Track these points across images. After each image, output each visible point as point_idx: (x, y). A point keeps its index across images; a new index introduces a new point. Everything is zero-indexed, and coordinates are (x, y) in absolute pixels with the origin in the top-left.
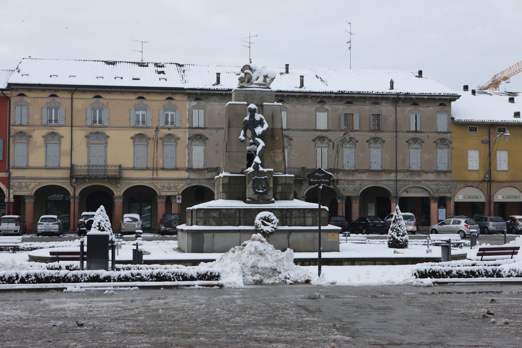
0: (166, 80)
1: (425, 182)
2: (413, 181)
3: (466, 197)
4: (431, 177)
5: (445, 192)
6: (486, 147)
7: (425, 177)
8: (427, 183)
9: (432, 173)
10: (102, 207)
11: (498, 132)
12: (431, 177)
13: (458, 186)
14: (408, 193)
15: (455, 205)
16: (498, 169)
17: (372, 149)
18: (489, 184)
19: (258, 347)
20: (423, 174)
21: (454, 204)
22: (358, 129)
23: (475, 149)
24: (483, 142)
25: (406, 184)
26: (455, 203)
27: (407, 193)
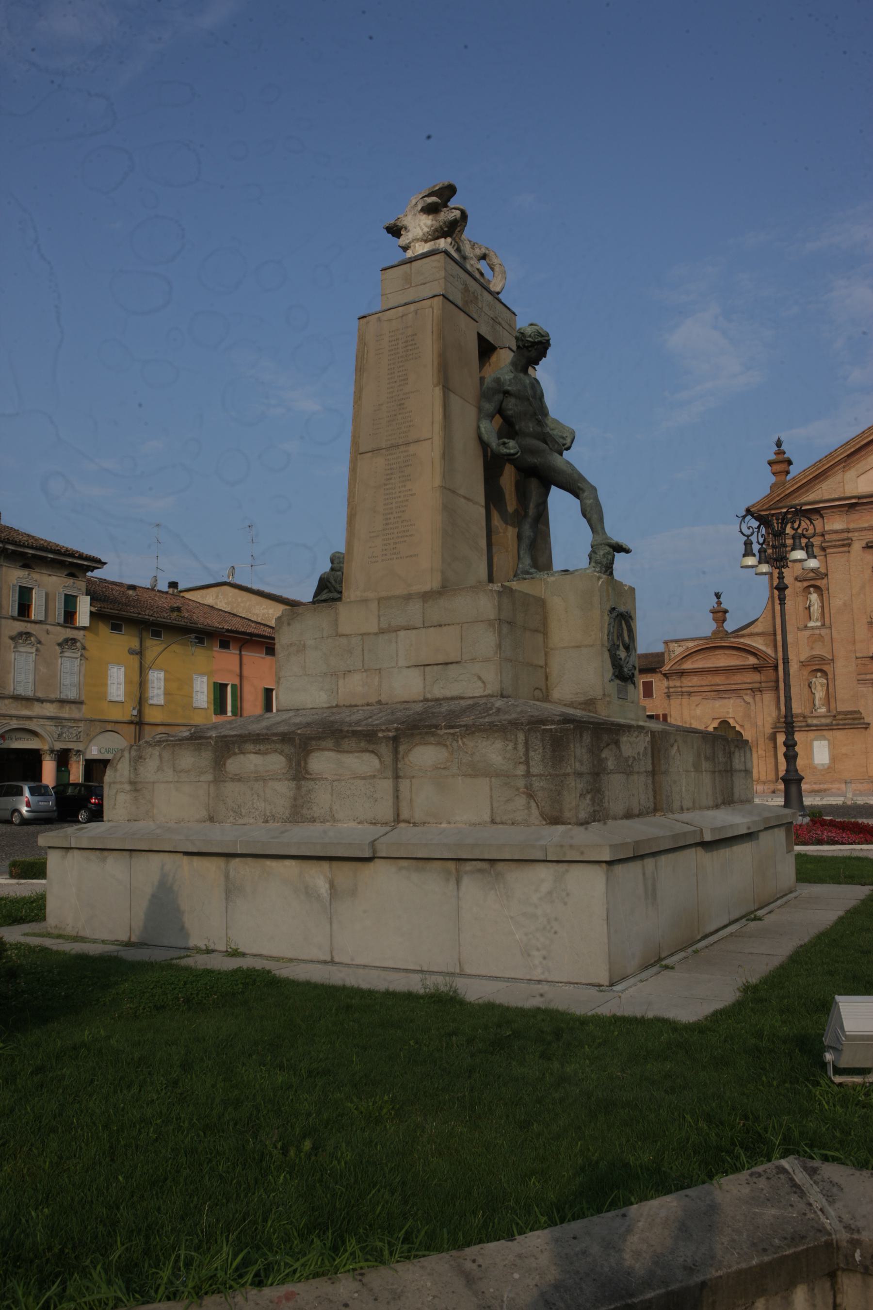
0: (737, 516)
1: (39, 720)
2: (18, 717)
3: (103, 750)
4: (50, 710)
5: (71, 740)
6: (134, 660)
7: (38, 709)
8: (42, 722)
9: (51, 701)
10: (838, 998)
11: (652, 681)
12: (50, 710)
13: (91, 730)
14: (6, 741)
15: (85, 765)
16: (195, 705)
17: (66, 659)
18: (138, 727)
19: (87, 1309)
20: (36, 703)
21: (84, 763)
22: (42, 617)
23: (119, 664)
24: (132, 652)
25: (5, 722)
26: (86, 760)
27: (4, 740)
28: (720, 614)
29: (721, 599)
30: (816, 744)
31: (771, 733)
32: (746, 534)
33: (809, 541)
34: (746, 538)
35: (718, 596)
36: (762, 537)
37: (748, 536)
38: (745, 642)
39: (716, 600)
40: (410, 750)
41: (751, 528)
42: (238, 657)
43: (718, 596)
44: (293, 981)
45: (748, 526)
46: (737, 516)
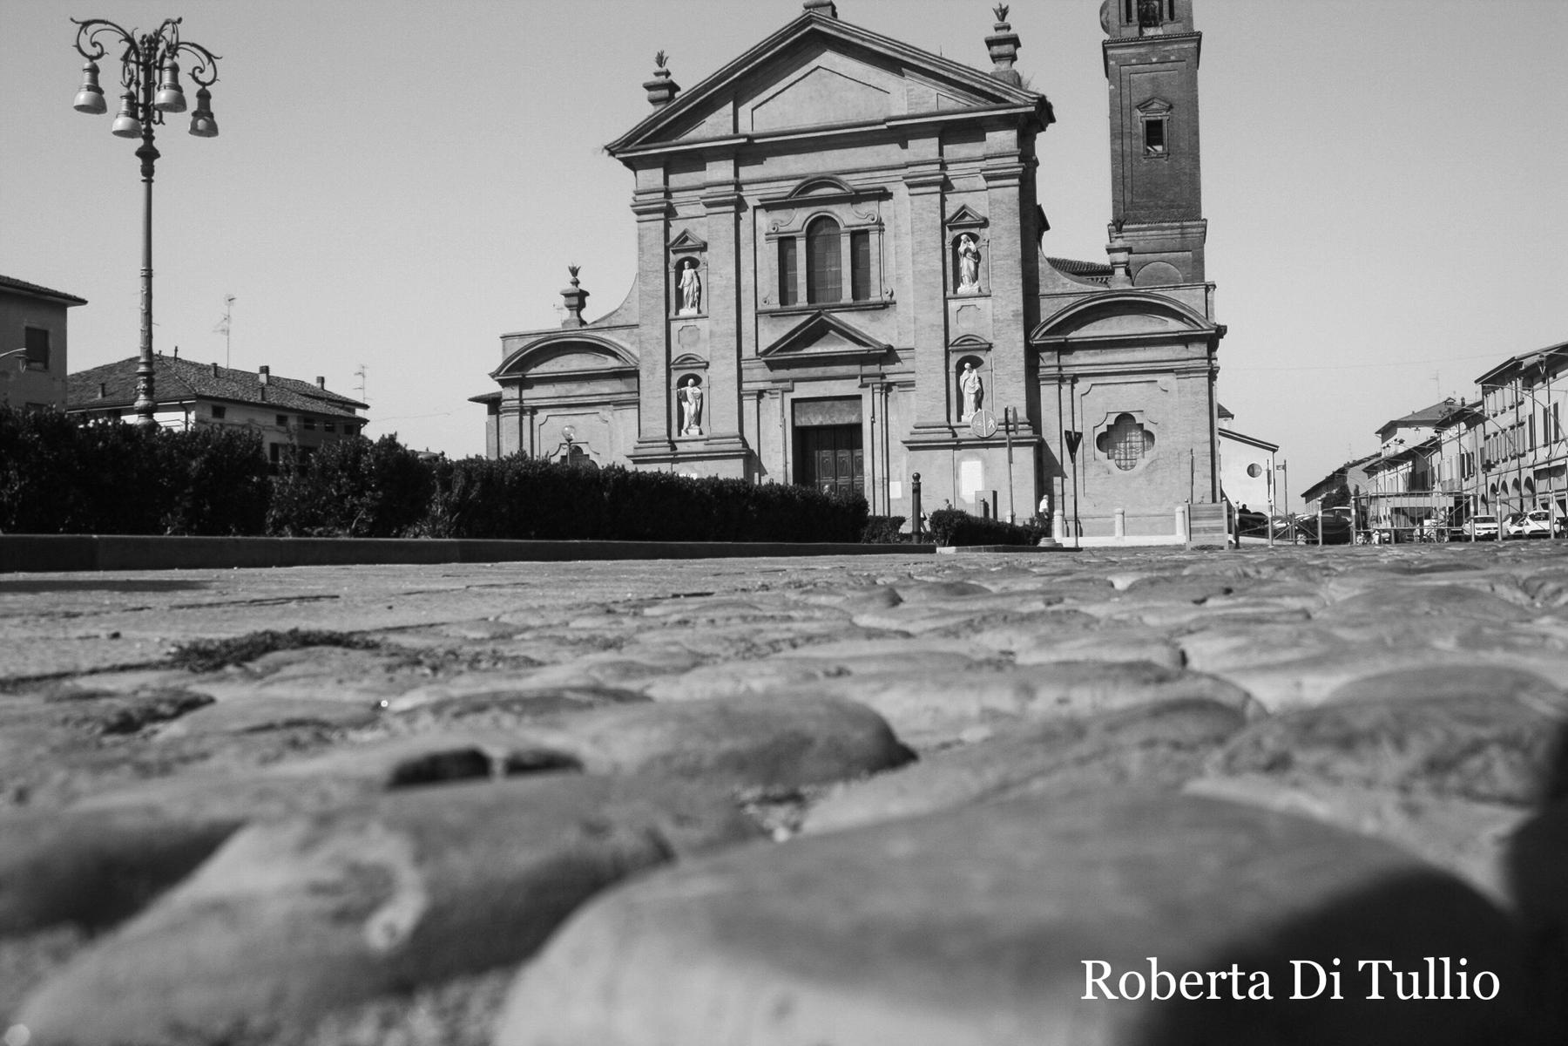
0: (72, 20)
28: (578, 299)
29: (579, 277)
30: (742, 477)
31: (961, 514)
32: (89, 53)
33: (204, 88)
34: (200, 87)
35: (574, 272)
36: (129, 74)
37: (92, 58)
38: (604, 337)
39: (571, 278)
40: (1446, 651)
41: (98, 47)
42: (637, 410)
43: (574, 272)
44: (64, 589)
45: (93, 40)
46: (72, 20)
